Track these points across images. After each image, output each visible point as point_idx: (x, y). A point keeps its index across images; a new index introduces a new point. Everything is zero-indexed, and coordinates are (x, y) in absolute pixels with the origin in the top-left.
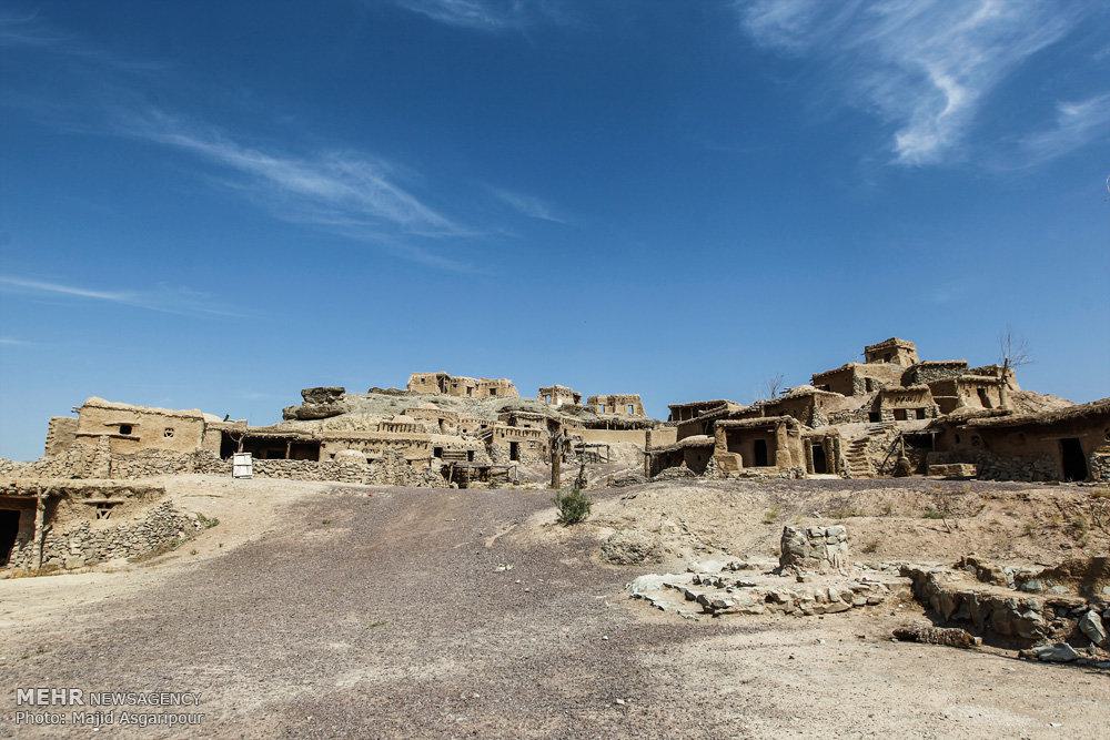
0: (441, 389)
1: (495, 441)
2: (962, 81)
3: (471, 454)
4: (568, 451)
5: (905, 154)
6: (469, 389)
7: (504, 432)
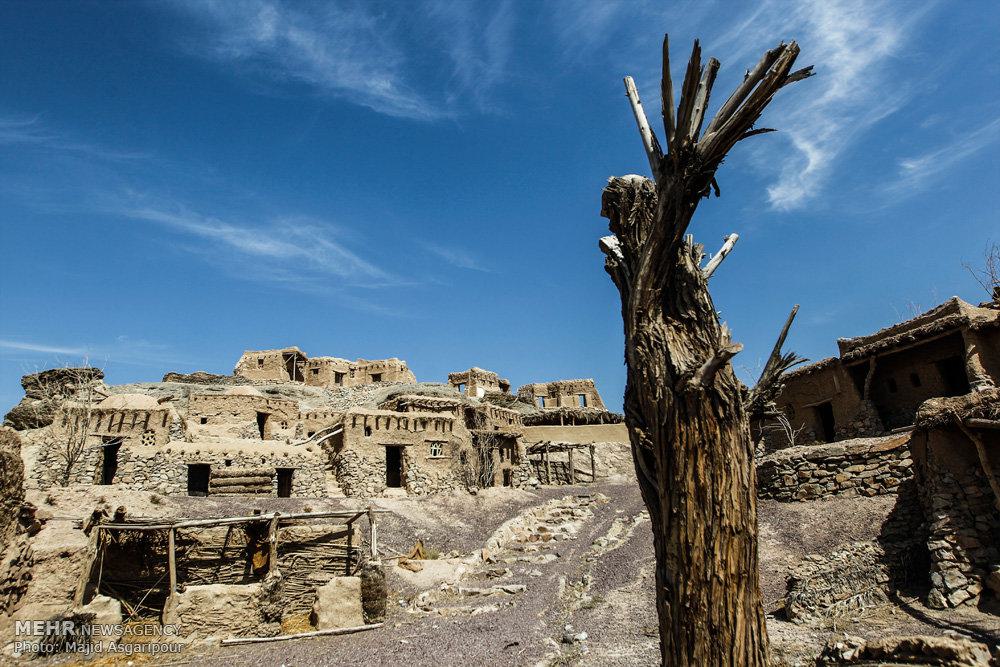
0: (290, 371)
1: (349, 445)
2: (819, 146)
3: (285, 477)
4: (515, 460)
5: (777, 203)
6: (339, 377)
7: (371, 423)
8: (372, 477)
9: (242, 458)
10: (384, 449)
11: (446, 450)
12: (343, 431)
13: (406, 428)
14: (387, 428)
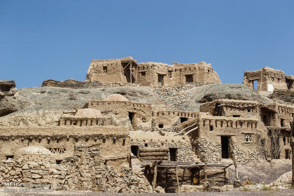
1: (202, 136)
3: (173, 152)
6: (161, 77)
8: (215, 153)
9: (154, 144)
10: (220, 138)
11: (254, 139)
12: (199, 128)
13: (232, 126)
14: (222, 126)
